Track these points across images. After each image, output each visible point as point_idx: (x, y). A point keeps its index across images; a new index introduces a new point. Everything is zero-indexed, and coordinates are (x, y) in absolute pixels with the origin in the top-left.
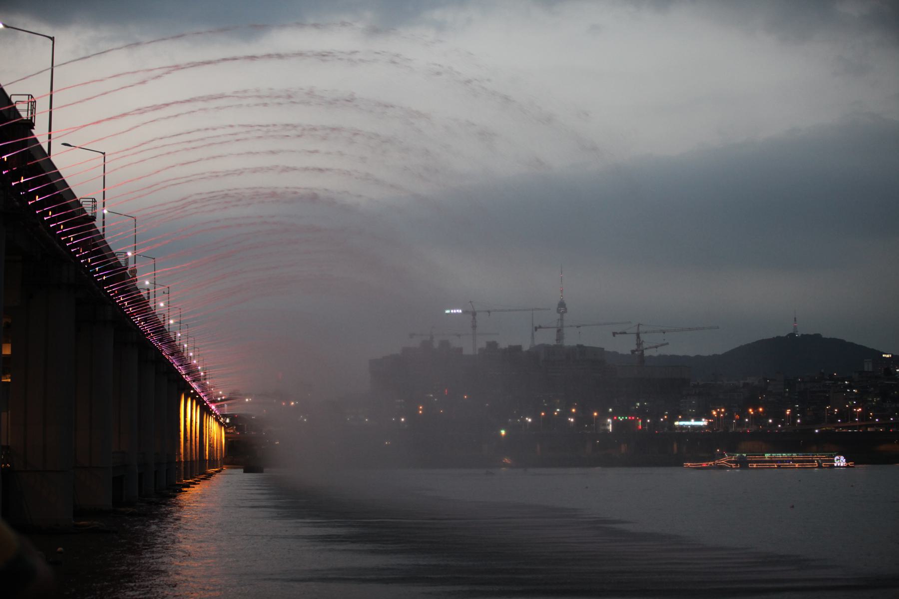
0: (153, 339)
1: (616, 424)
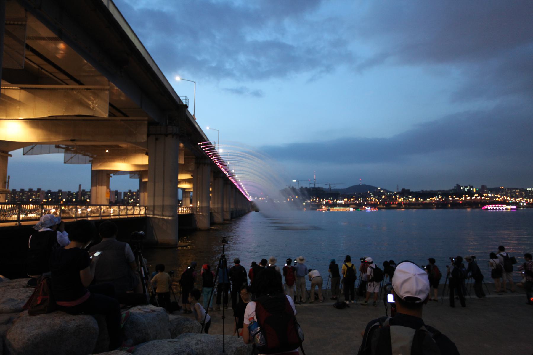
0: (238, 187)
1: (326, 202)
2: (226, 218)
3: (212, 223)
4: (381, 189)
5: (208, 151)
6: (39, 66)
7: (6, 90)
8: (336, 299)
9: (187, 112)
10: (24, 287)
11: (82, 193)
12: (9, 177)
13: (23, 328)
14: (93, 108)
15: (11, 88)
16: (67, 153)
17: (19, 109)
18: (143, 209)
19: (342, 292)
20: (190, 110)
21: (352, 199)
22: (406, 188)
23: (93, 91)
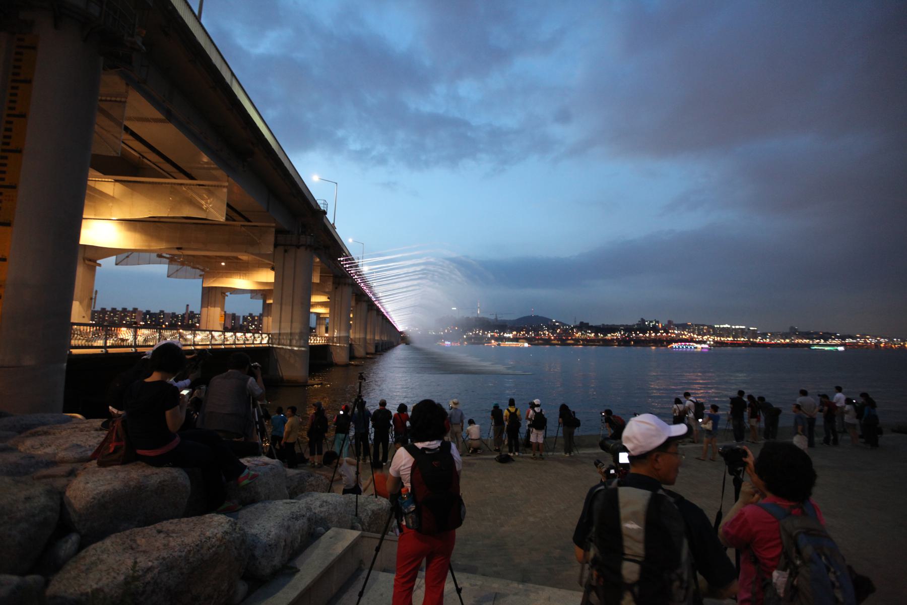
1: (491, 335)
2: (369, 351)
3: (352, 357)
4: (557, 322)
5: (350, 269)
6: (139, 154)
7: (97, 182)
8: (498, 450)
9: (325, 220)
10: (96, 430)
11: (189, 315)
12: (96, 291)
13: (88, 483)
14: (207, 208)
15: (103, 180)
16: (172, 264)
17: (112, 206)
18: (266, 337)
19: (506, 443)
20: (330, 216)
21: (522, 333)
22: (585, 321)
23: (207, 187)
